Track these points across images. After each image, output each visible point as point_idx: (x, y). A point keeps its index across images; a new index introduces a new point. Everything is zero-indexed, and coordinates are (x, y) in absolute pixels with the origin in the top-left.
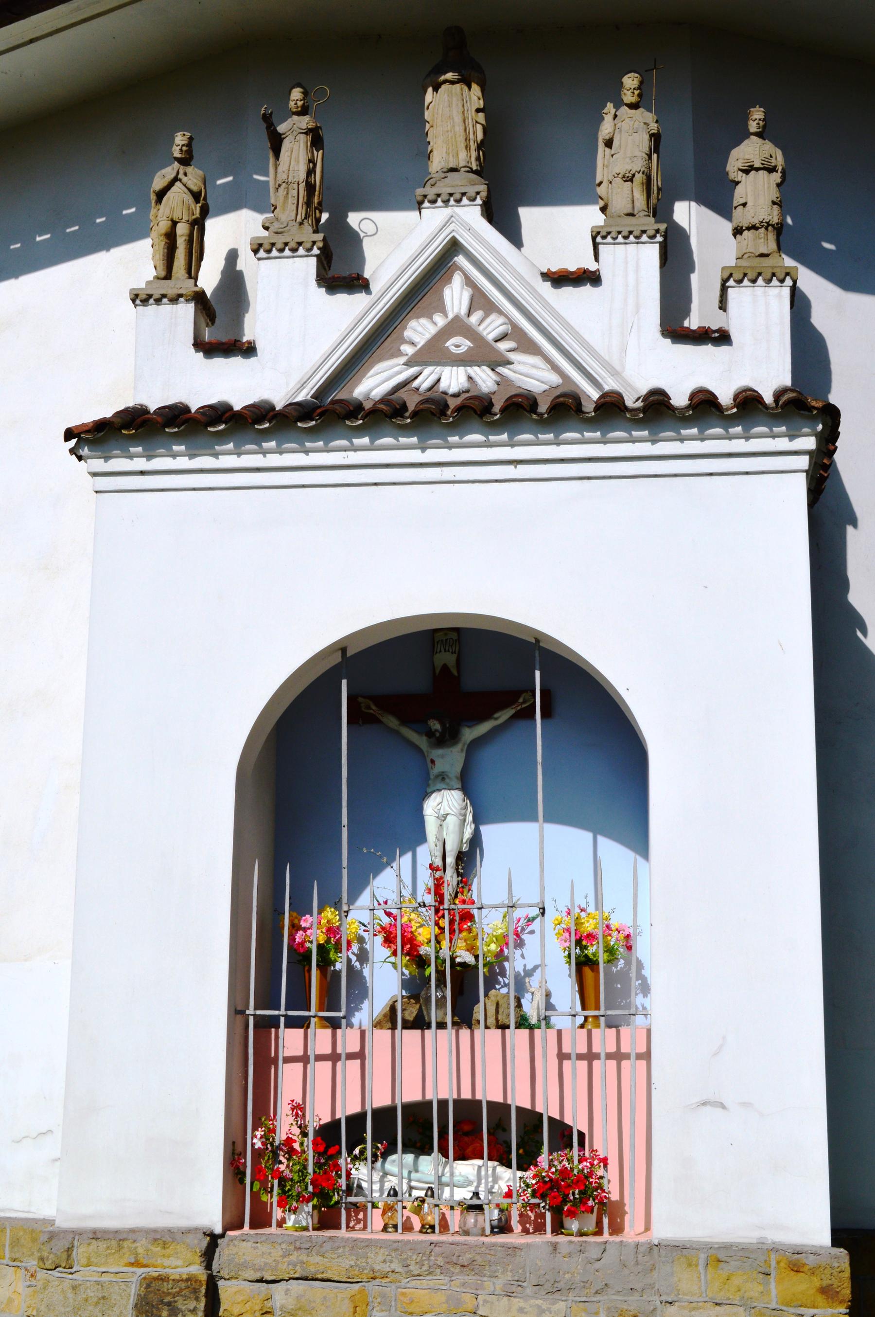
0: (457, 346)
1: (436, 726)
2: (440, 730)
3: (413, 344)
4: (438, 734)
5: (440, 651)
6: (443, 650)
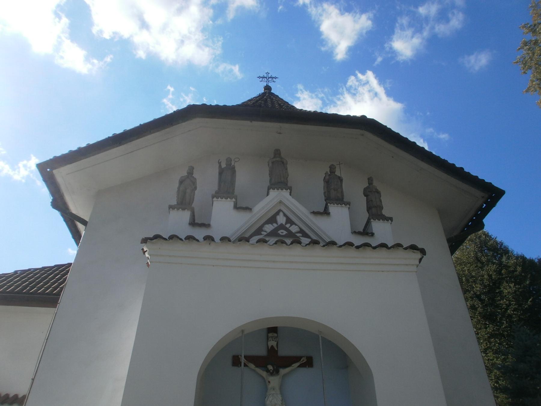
0: (282, 233)
1: (270, 367)
2: (273, 369)
3: (266, 232)
4: (271, 371)
5: (271, 340)
6: (272, 340)
